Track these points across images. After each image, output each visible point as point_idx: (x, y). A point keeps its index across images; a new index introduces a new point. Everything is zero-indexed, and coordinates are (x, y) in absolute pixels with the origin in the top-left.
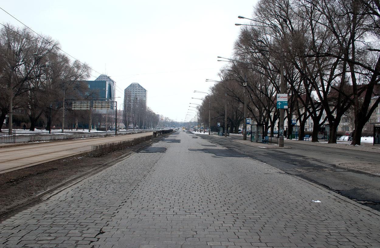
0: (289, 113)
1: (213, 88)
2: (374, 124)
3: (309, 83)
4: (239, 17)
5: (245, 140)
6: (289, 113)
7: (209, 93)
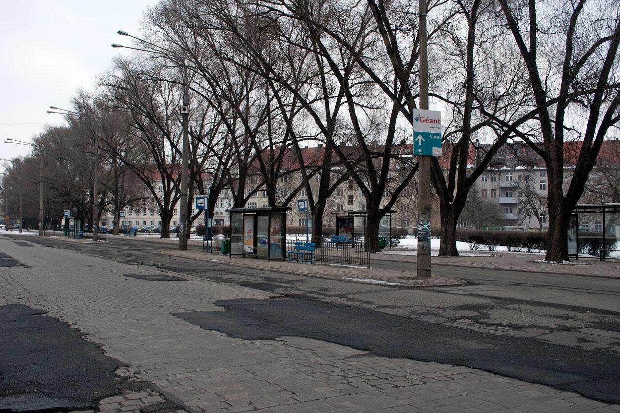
0: (163, 204)
1: (37, 140)
2: (337, 214)
3: (235, 152)
4: (120, 33)
5: (183, 250)
6: (163, 204)
7: (26, 151)
